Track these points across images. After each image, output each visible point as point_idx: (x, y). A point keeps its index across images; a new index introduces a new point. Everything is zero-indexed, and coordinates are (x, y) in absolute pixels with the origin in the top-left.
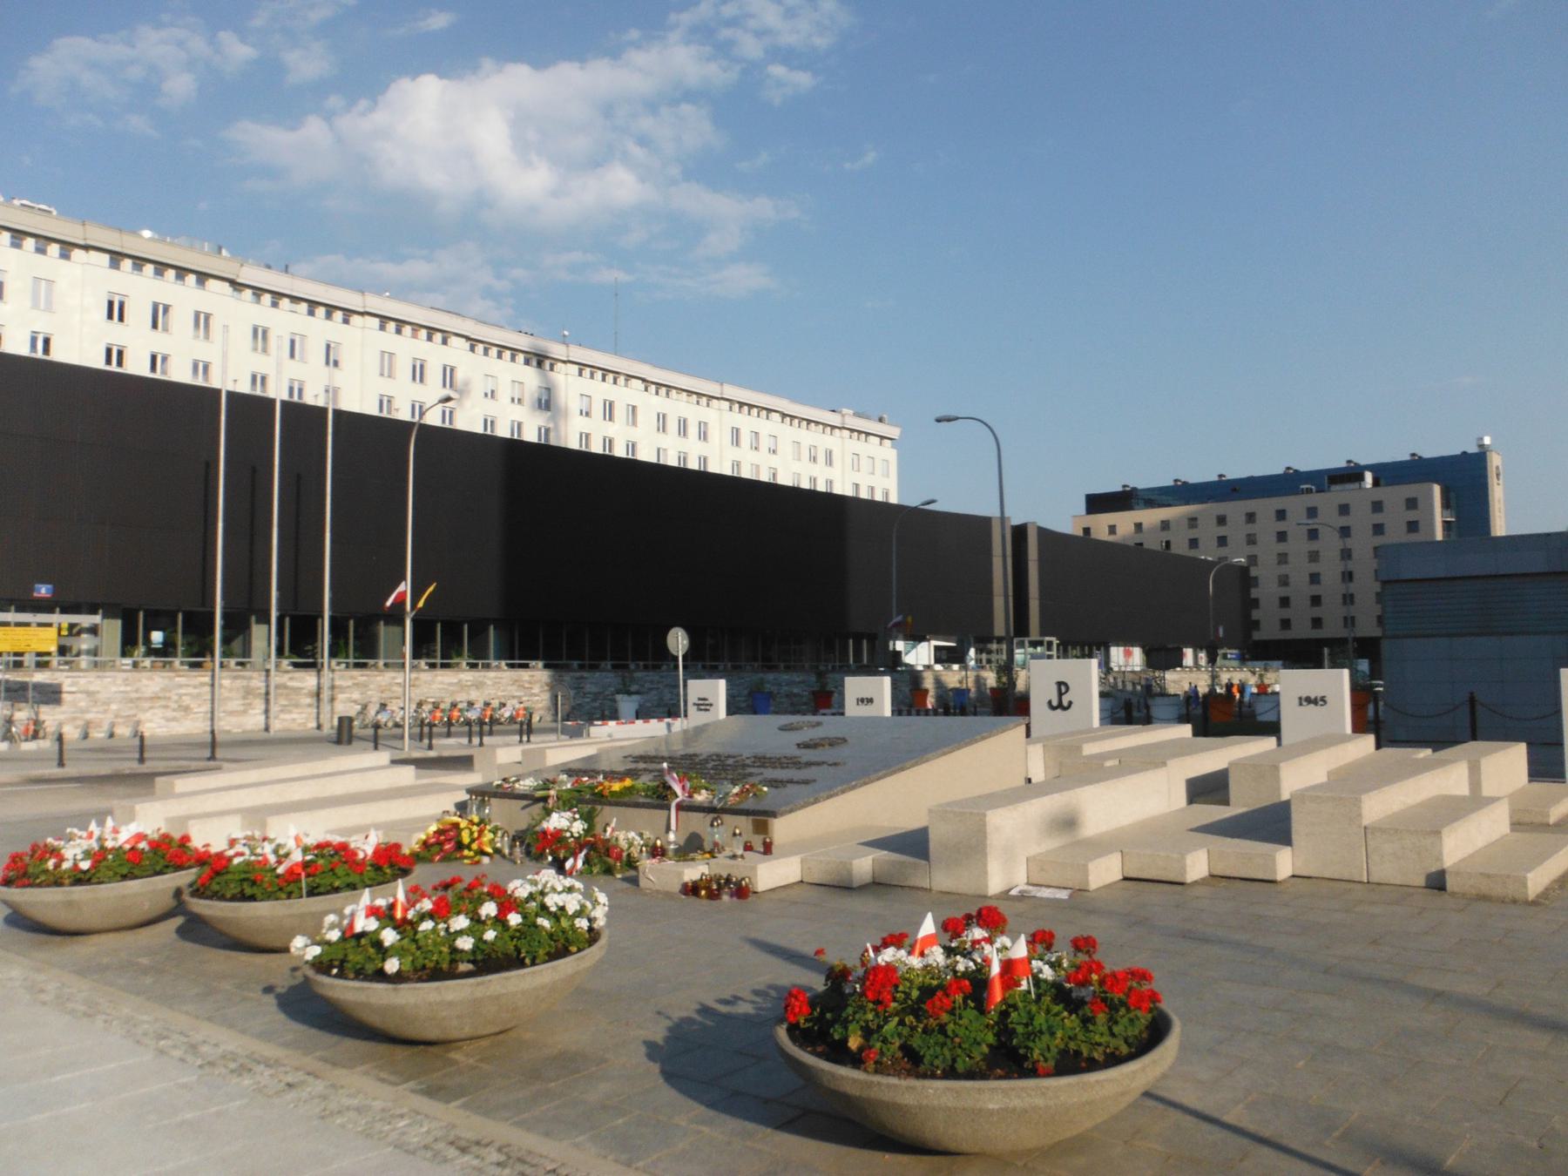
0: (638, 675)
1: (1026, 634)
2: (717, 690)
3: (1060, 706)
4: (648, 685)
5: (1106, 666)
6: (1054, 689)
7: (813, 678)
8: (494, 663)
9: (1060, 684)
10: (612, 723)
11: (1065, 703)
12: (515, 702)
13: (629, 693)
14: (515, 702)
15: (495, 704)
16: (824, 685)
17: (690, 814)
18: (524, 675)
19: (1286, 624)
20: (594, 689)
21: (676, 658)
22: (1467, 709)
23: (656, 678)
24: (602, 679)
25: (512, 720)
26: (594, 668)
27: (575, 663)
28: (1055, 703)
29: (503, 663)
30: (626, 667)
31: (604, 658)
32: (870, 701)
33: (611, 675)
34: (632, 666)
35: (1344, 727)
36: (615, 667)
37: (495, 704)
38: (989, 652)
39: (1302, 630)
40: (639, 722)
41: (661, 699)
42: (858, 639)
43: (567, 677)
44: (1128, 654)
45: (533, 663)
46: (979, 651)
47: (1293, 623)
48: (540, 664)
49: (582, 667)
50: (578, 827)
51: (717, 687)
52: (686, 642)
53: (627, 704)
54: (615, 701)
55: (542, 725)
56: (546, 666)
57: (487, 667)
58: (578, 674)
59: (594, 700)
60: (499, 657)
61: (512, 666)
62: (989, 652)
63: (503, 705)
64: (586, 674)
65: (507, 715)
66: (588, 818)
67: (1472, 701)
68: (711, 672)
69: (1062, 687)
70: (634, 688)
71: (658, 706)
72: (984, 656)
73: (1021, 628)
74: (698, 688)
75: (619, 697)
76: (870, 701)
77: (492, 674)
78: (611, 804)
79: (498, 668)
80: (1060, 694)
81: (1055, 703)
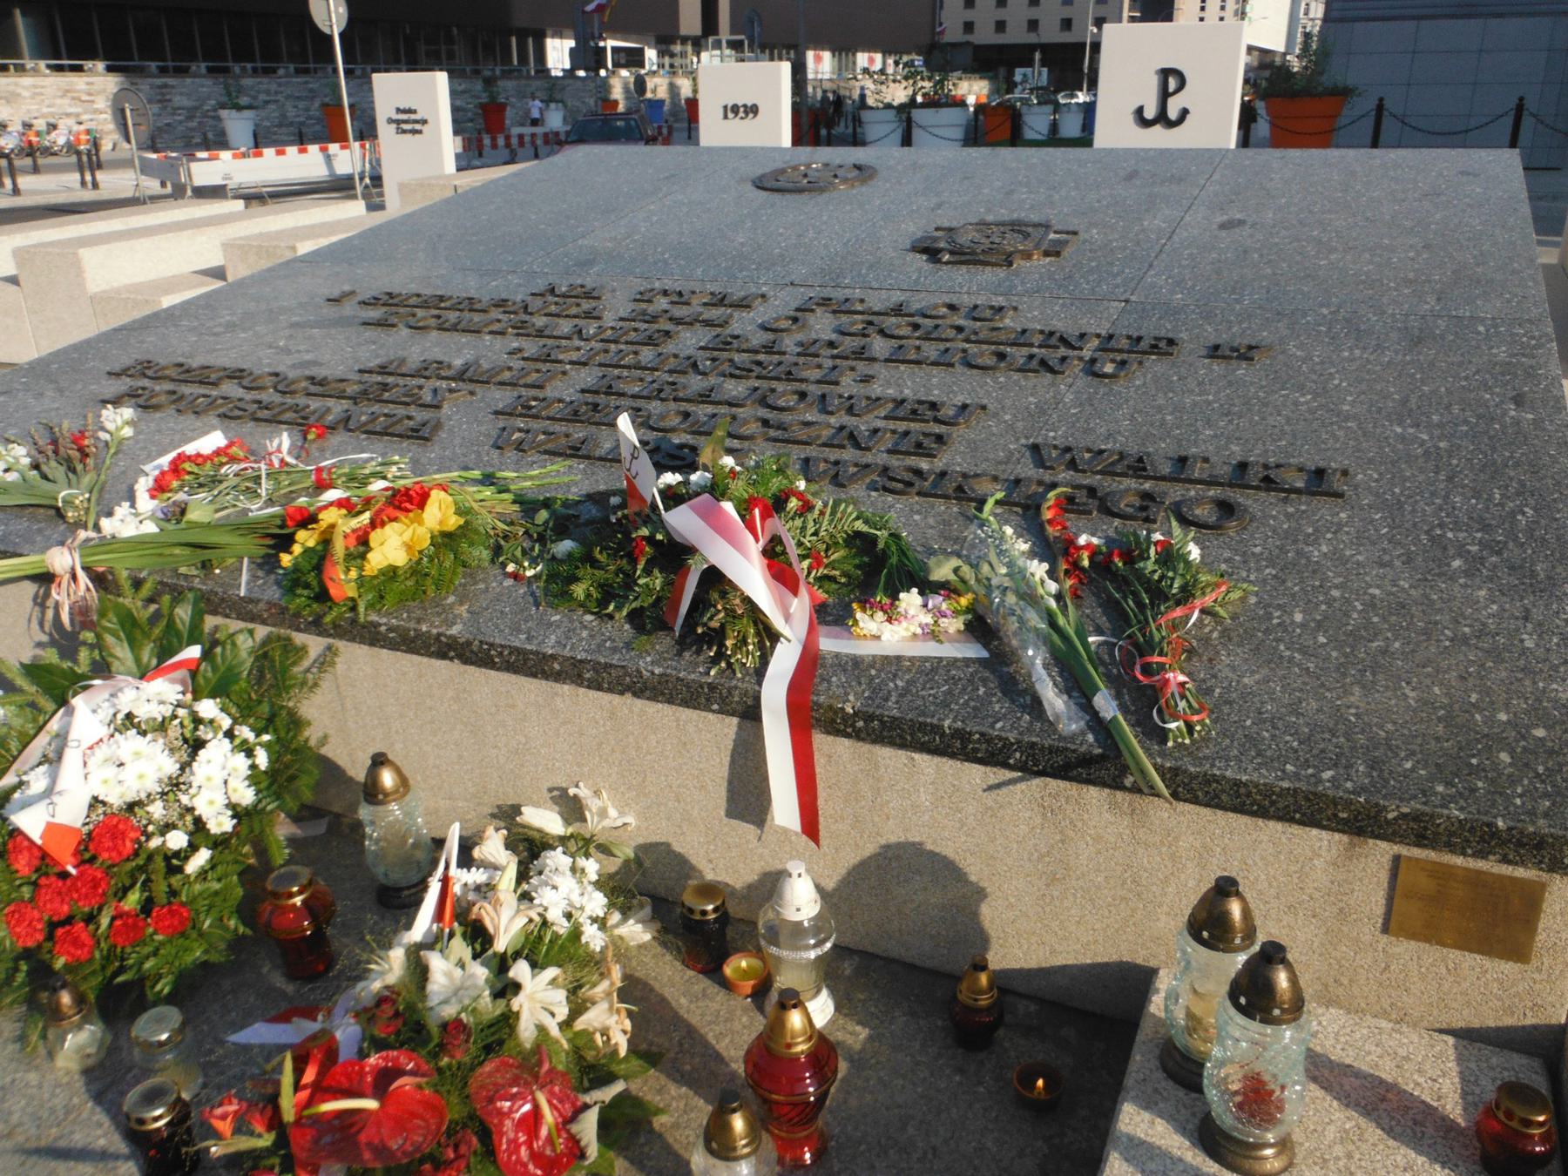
0: (248, 82)
1: (715, 32)
2: (432, 92)
3: (1162, 118)
4: (262, 97)
5: (799, 71)
6: (1153, 82)
7: (478, 86)
8: (30, 64)
9: (1166, 73)
10: (226, 155)
11: (1173, 114)
12: (71, 122)
13: (239, 108)
14: (71, 122)
15: (40, 125)
16: (493, 97)
17: (889, 758)
18: (78, 82)
19: (1001, 26)
20: (186, 102)
21: (330, 38)
22: (1509, 121)
23: (274, 87)
24: (194, 88)
25: (71, 148)
26: (181, 72)
27: (153, 65)
28: (1150, 113)
29: (42, 64)
30: (226, 70)
31: (194, 58)
32: (752, 110)
33: (209, 82)
34: (237, 70)
35: (1229, 141)
36: (210, 70)
37: (40, 125)
38: (672, 55)
39: (985, 35)
40: (269, 152)
41: (284, 116)
42: (522, 35)
43: (145, 85)
44: (818, 59)
45: (88, 64)
46: (661, 54)
47: (976, 26)
48: (101, 66)
49: (163, 71)
50: (223, 780)
51: (434, 85)
52: (343, 10)
53: (238, 125)
54: (219, 119)
55: (118, 155)
56: (110, 69)
57: (21, 69)
58: (159, 81)
59: (190, 118)
60: (40, 54)
61: (59, 69)
62: (672, 55)
63: (53, 127)
64: (171, 81)
65: (61, 141)
66: (262, 697)
67: (1520, 109)
68: (412, 60)
69: (1171, 79)
70: (244, 101)
71: (280, 125)
72: (667, 60)
73: (710, 24)
74: (392, 89)
75: (224, 113)
76: (752, 110)
77: (26, 81)
78: (371, 636)
79: (35, 71)
80: (1165, 95)
81: (1150, 113)
